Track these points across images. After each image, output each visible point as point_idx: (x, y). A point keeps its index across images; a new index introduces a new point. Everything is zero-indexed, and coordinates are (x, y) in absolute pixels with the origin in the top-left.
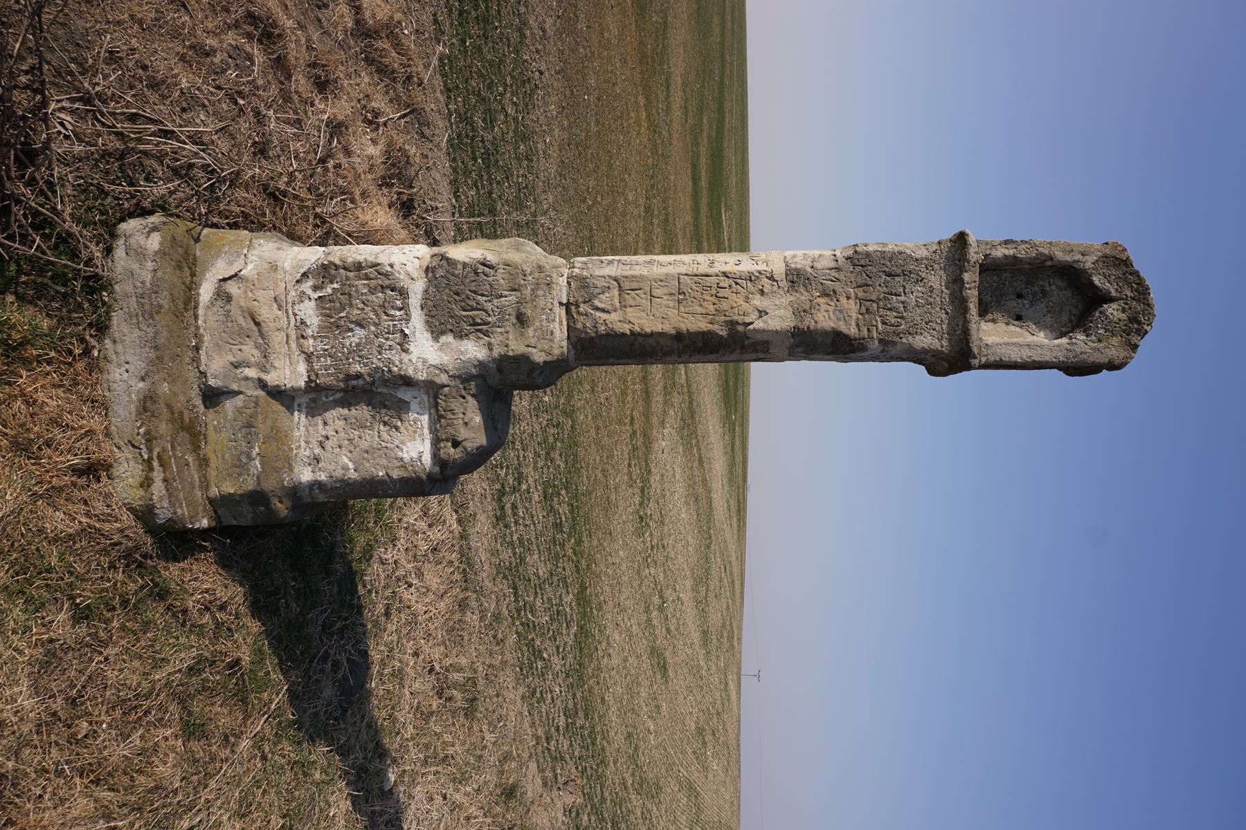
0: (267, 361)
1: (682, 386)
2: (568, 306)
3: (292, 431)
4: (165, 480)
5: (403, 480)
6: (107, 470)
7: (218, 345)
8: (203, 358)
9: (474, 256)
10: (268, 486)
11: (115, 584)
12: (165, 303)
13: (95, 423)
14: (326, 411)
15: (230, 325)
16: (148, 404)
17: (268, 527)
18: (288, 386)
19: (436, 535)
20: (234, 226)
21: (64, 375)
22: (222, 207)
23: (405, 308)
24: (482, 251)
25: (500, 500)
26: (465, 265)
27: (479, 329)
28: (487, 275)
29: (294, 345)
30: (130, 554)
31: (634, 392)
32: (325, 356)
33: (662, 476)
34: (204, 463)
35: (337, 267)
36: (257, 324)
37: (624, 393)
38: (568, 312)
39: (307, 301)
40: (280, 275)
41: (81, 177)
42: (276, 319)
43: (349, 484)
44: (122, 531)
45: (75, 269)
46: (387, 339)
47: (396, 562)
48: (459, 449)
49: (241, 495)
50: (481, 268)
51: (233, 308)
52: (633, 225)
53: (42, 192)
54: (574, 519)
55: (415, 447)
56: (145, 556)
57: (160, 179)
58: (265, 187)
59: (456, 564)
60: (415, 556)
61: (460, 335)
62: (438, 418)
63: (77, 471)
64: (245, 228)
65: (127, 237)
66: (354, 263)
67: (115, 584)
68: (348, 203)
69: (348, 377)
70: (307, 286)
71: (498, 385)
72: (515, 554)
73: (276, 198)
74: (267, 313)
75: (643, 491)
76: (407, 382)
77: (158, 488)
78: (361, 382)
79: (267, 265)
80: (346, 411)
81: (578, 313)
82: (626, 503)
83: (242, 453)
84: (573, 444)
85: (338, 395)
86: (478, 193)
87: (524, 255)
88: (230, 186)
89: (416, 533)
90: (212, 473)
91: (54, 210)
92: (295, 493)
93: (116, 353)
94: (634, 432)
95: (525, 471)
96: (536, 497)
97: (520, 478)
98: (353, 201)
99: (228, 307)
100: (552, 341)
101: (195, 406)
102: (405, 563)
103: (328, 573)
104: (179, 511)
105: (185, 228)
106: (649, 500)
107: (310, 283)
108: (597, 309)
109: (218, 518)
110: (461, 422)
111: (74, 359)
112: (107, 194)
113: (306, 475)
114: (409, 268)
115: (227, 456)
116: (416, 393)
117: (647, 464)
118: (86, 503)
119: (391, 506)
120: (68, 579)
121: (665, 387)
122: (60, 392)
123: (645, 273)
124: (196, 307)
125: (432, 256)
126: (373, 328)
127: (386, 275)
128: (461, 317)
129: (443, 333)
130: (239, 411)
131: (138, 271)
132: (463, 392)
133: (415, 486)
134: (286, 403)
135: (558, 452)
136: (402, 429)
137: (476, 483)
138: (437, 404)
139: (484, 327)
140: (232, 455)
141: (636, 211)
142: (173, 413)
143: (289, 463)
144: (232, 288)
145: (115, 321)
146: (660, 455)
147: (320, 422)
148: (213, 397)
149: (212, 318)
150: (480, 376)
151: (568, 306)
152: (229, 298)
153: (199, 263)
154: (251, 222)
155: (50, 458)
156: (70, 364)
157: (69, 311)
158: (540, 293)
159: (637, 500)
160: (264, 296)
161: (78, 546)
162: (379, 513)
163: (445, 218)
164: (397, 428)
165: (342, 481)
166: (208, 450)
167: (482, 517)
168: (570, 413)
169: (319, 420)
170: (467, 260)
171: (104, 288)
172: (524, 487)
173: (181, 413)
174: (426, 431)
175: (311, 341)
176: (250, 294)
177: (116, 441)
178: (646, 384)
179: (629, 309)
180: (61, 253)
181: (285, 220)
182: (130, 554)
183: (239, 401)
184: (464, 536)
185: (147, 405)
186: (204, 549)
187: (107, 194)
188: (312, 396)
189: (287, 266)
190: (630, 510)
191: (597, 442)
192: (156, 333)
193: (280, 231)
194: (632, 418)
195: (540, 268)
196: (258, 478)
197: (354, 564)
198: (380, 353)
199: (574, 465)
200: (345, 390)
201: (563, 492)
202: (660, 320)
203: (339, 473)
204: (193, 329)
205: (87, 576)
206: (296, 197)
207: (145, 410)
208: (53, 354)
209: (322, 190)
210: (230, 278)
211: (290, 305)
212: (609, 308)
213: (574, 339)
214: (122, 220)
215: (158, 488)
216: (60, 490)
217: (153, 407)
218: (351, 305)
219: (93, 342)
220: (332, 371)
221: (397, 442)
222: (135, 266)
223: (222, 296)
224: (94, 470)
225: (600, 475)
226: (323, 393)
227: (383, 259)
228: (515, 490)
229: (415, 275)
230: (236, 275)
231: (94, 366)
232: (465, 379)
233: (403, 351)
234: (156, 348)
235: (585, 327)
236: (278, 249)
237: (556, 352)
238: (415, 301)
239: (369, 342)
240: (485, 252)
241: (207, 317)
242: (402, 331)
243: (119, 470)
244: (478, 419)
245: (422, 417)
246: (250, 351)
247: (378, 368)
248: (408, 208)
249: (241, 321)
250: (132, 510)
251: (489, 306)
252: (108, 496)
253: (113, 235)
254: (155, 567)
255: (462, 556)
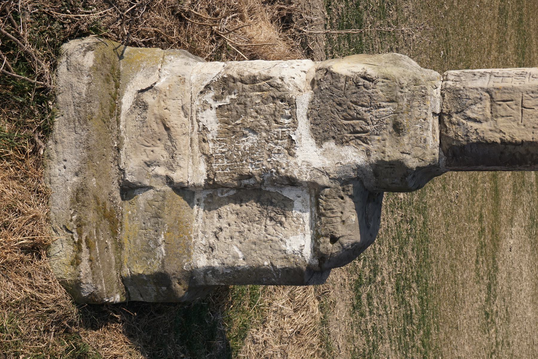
0: (174, 161)
1: (532, 185)
2: (441, 116)
3: (191, 222)
4: (90, 260)
5: (286, 271)
6: (46, 249)
7: (135, 147)
8: (123, 157)
9: (356, 70)
10: (171, 269)
11: (48, 345)
12: (96, 110)
13: (39, 211)
14: (221, 205)
15: (145, 129)
16: (80, 195)
17: (167, 304)
18: (191, 183)
19: (300, 319)
20: (148, 44)
21: (18, 169)
22: (140, 28)
23: (293, 116)
24: (363, 66)
25: (357, 290)
26: (347, 78)
27: (359, 136)
28: (367, 88)
29: (196, 148)
30: (60, 321)
31: (484, 190)
32: (222, 158)
33: (509, 273)
34: (119, 246)
35: (235, 80)
36: (167, 129)
37: (474, 191)
38: (441, 121)
39: (208, 110)
40: (187, 87)
41: (37, 7)
42: (183, 125)
43: (238, 271)
44: (55, 301)
45: (30, 83)
46: (276, 144)
47: (265, 342)
48: (337, 244)
49: (147, 276)
50: (362, 81)
51: (149, 115)
52: (487, 28)
53: (10, 21)
54: (423, 312)
55: (297, 241)
56: (70, 323)
57: (94, 6)
58: (173, 10)
59: (317, 347)
60: (281, 337)
61: (342, 142)
62: (318, 215)
63: (25, 250)
64: (157, 46)
65: (69, 56)
66: (250, 77)
67: (48, 345)
68: (238, 19)
69: (242, 177)
70: (209, 97)
71: (372, 187)
72: (368, 341)
73: (179, 17)
74: (176, 119)
75: (489, 287)
76: (292, 182)
77: (85, 266)
78: (252, 181)
79: (176, 78)
80: (238, 207)
81: (451, 122)
82: (473, 298)
83: (150, 239)
84: (424, 240)
85: (232, 193)
86: (347, 6)
87: (401, 69)
88: (146, 10)
89: (283, 316)
90: (125, 255)
91: (17, 34)
92: (191, 276)
93: (57, 152)
94: (483, 230)
95: (380, 263)
96: (389, 289)
97: (375, 271)
98: (242, 18)
99: (144, 114)
100: (425, 148)
101: (114, 198)
102: (273, 343)
103: (210, 348)
104: (100, 287)
105: (112, 47)
106: (495, 297)
107: (212, 94)
108: (469, 119)
109: (128, 294)
110: (339, 220)
111: (26, 157)
112: (54, 20)
113: (201, 261)
114: (298, 81)
115: (138, 241)
116: (299, 192)
117: (494, 261)
118: (30, 276)
119: (263, 291)
120: (15, 339)
121: (514, 186)
122: (15, 183)
123: (517, 85)
124: (118, 114)
125: (317, 70)
126: (264, 134)
127: (277, 87)
128: (343, 125)
129: (326, 139)
130: (149, 203)
131: (76, 84)
132: (342, 193)
133: (294, 276)
134: (188, 197)
135: (410, 247)
136: (286, 225)
137: (337, 276)
138: (318, 204)
139: (363, 135)
140: (142, 240)
141: (490, 14)
142: (98, 204)
143: (188, 251)
144: (148, 97)
145: (56, 126)
146: (507, 253)
147: (216, 216)
148: (128, 190)
149: (131, 124)
150: (358, 178)
151: (441, 116)
152: (145, 107)
153: (122, 78)
154: (161, 41)
155: (6, 238)
156: (23, 161)
157: (25, 118)
158: (415, 104)
159: (484, 296)
160: (174, 105)
161: (22, 311)
162: (253, 296)
163: (321, 31)
164: (281, 224)
165: (233, 268)
166: (123, 236)
167: (340, 305)
168: (422, 210)
169: (215, 213)
170: (349, 74)
171: (50, 98)
172: (379, 279)
173: (104, 204)
174: (307, 227)
175: (211, 145)
176: (162, 103)
177: (54, 225)
178: (495, 183)
179: (500, 119)
180: (20, 70)
181: (188, 37)
182: (60, 321)
183: (149, 194)
184: (324, 322)
185: (79, 196)
186: (115, 320)
187: (54, 20)
188: (210, 192)
189: (193, 79)
190: (476, 305)
191: (447, 238)
192: (88, 136)
193: (185, 47)
194: (481, 216)
195: (416, 81)
196: (163, 262)
197: (230, 342)
198: (270, 156)
199: (425, 259)
200: (237, 188)
201: (414, 285)
202: (531, 130)
203: (229, 261)
204: (116, 132)
205: (27, 337)
206: (197, 16)
207: (78, 200)
208: (11, 152)
209: (218, 9)
210: (147, 89)
211: (194, 113)
212: (481, 118)
213: (445, 147)
214: (65, 41)
215: (85, 266)
216: (12, 264)
217: (84, 198)
218: (246, 114)
219: (40, 142)
220: (228, 171)
221: (281, 236)
222: (74, 80)
223: (140, 105)
224: (36, 249)
225: (448, 271)
226: (219, 191)
227: (274, 73)
228: (370, 281)
229: (302, 87)
230: (151, 87)
231: (39, 163)
232: (344, 181)
233: (290, 155)
234: (88, 148)
235: (457, 135)
236: (186, 64)
237: (429, 158)
238: (302, 110)
239: (260, 146)
240: (366, 67)
241: (128, 123)
242: (290, 137)
243: (55, 250)
244: (354, 218)
245: (304, 215)
246: (160, 152)
247: (267, 169)
248: (287, 22)
249: (155, 126)
250: (63, 283)
251: (368, 116)
252: (46, 270)
253: (58, 54)
254: (77, 333)
255: (322, 340)
